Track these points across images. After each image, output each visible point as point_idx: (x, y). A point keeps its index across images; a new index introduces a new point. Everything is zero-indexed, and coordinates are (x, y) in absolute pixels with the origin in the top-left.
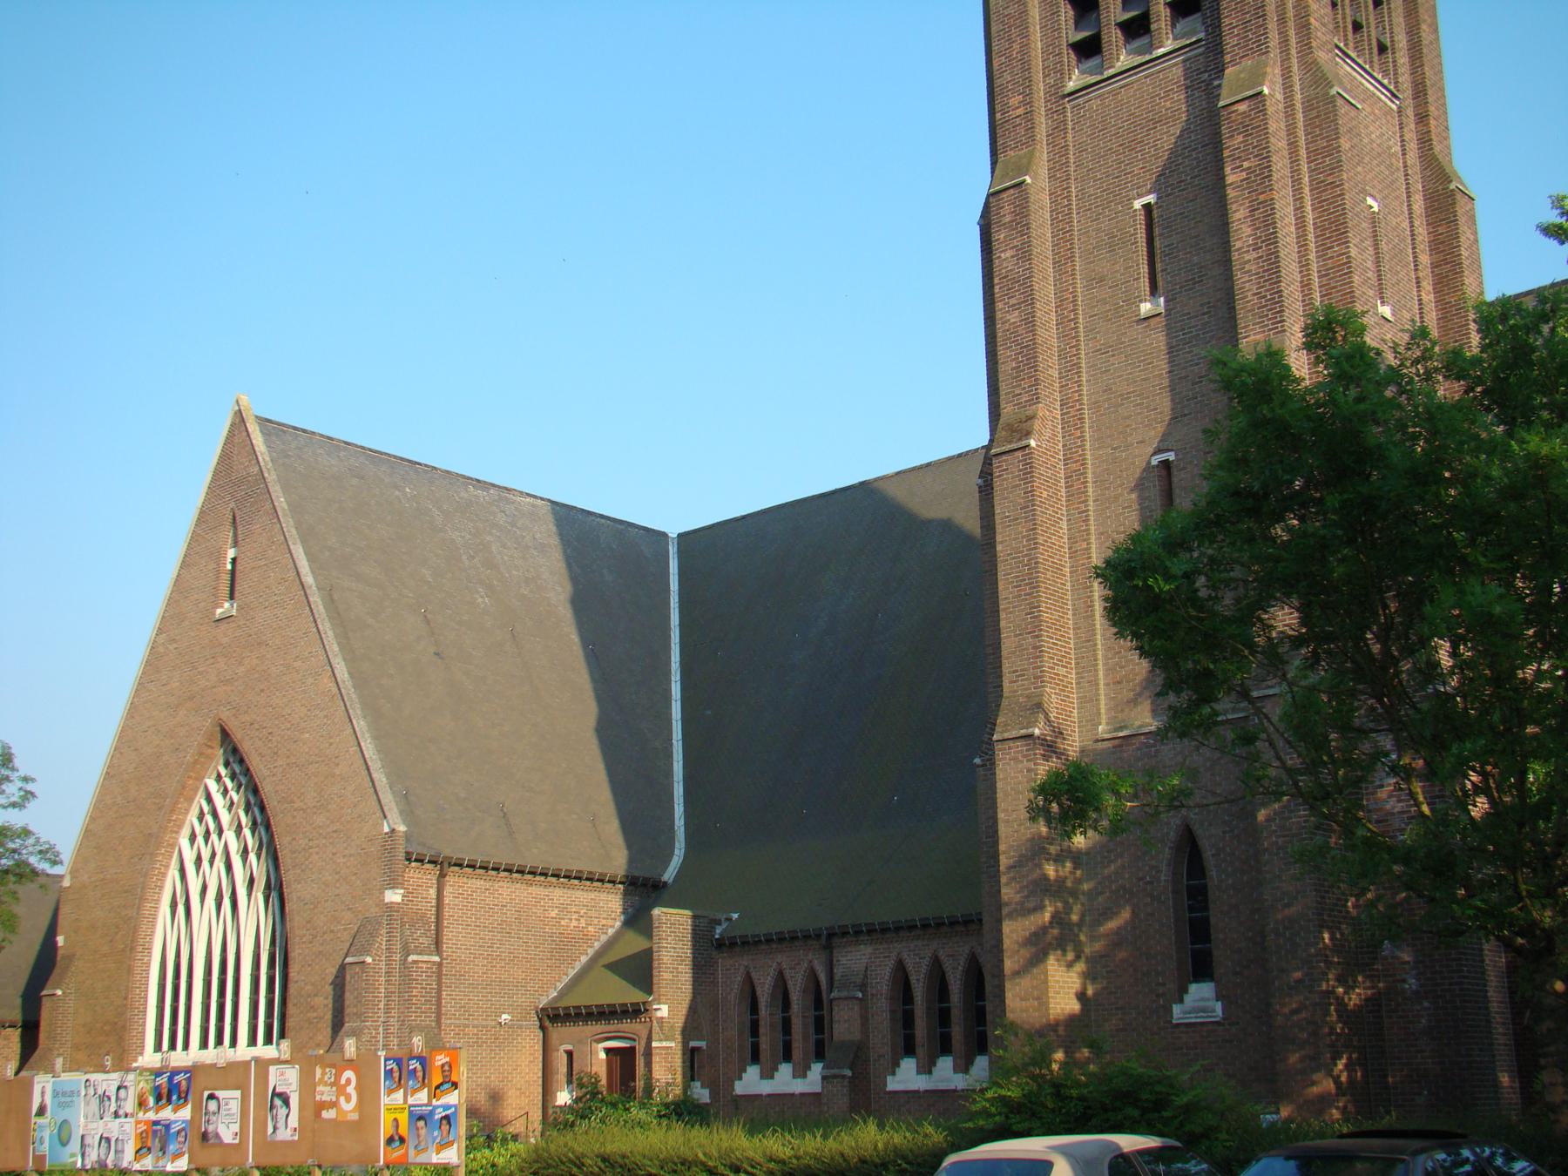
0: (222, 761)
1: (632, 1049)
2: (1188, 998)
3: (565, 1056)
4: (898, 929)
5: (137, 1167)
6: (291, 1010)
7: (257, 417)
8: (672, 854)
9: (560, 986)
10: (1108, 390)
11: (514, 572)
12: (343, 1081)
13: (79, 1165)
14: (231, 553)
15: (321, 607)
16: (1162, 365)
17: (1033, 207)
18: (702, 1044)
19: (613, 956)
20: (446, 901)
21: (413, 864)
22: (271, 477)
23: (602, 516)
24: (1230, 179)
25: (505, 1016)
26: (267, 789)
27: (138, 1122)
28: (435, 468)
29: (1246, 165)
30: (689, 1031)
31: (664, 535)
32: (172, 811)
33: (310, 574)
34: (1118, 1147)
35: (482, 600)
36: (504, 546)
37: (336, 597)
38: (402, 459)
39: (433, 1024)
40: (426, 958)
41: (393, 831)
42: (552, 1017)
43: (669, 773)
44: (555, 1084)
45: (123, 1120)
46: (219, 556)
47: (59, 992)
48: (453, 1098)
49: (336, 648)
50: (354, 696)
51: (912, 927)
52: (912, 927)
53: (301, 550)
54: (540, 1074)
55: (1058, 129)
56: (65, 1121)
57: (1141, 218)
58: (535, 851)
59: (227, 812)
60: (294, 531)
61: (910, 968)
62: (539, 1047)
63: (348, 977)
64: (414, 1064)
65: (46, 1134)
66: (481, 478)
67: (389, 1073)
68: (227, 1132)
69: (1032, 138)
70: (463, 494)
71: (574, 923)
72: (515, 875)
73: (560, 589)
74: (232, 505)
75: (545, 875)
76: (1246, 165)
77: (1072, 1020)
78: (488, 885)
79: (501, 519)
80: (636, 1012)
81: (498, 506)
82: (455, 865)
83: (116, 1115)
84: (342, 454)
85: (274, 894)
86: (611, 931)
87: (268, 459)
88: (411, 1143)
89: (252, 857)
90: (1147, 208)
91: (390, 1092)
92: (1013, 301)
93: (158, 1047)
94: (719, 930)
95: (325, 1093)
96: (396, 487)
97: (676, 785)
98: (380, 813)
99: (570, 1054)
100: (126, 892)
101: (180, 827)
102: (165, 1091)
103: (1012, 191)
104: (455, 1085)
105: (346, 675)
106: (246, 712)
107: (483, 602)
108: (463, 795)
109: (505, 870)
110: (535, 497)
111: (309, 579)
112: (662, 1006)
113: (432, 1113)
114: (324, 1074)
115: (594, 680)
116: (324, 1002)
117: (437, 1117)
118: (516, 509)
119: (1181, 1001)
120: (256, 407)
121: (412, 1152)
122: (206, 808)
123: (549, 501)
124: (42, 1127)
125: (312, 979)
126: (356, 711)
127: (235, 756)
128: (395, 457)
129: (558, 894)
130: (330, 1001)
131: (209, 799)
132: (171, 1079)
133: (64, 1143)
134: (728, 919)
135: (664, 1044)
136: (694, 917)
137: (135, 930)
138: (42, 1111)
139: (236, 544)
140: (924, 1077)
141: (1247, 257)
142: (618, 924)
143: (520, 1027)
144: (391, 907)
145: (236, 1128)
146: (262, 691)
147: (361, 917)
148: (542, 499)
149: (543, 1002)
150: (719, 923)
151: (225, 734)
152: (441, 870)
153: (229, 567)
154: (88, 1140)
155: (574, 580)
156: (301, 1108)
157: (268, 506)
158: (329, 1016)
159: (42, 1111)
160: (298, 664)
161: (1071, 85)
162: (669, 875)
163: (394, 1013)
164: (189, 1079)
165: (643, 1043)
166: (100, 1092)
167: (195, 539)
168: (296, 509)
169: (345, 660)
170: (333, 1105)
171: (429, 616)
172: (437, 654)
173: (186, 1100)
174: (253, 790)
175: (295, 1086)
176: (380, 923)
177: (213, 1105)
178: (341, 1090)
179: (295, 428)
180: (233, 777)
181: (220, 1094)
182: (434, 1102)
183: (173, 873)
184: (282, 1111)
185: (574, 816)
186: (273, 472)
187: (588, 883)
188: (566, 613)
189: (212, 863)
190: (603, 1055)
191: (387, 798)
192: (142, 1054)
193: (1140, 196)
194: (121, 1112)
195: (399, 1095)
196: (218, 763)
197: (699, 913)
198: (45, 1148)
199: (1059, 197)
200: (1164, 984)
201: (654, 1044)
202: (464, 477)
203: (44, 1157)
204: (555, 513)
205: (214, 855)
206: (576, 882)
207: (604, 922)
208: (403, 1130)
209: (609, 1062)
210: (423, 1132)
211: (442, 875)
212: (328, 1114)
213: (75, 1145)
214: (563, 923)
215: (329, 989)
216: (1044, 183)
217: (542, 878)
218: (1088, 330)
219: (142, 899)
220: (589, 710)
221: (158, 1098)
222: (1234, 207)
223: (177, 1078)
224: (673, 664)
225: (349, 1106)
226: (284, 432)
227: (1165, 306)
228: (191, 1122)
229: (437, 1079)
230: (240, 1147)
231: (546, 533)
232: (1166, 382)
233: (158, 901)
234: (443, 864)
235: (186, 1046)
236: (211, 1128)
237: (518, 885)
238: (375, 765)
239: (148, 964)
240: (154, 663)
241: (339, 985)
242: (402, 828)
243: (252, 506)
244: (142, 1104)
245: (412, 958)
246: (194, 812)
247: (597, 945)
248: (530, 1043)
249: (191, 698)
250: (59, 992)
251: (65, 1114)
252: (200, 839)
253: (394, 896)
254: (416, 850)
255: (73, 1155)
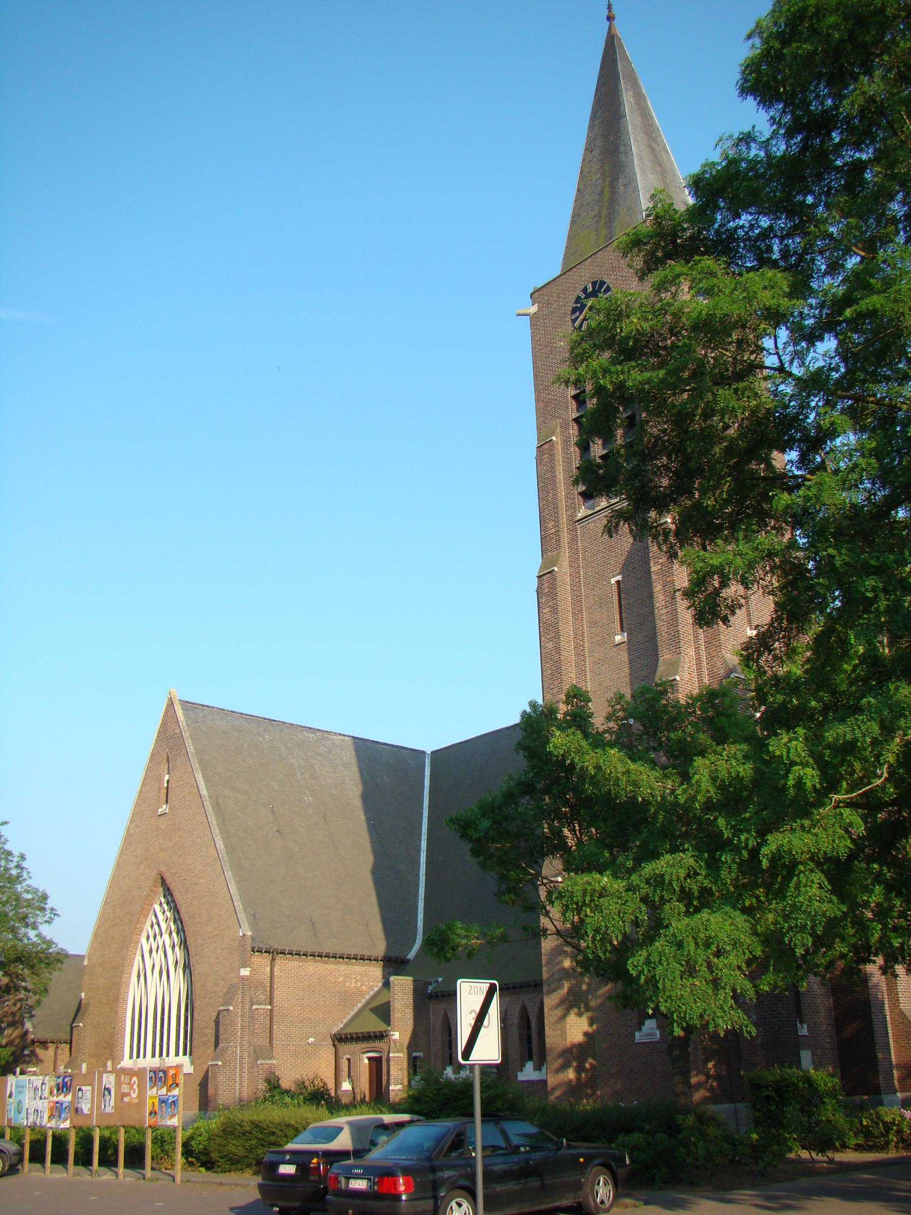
0: (162, 895)
1: (381, 1057)
2: (644, 1028)
3: (347, 1062)
4: (521, 987)
5: (49, 1125)
6: (195, 1036)
7: (180, 701)
8: (415, 942)
9: (345, 1021)
10: (600, 684)
11: (329, 781)
12: (132, 1082)
13: (25, 1124)
14: (167, 777)
15: (210, 808)
16: (627, 671)
17: (558, 584)
18: (421, 1054)
19: (375, 1004)
20: (276, 974)
21: (256, 953)
22: (186, 735)
23: (385, 744)
24: (653, 569)
25: (311, 1039)
26: (183, 910)
27: (50, 1102)
28: (284, 723)
29: (660, 561)
30: (411, 1047)
31: (424, 753)
32: (137, 923)
33: (205, 789)
34: (381, 1120)
35: (308, 798)
36: (323, 766)
37: (220, 802)
38: (265, 719)
39: (268, 1044)
40: (263, 1007)
41: (244, 935)
42: (340, 1039)
43: (416, 895)
44: (341, 1078)
45: (43, 1100)
46: (161, 779)
47: (81, 1025)
48: (176, 1092)
49: (217, 831)
50: (226, 858)
51: (529, 986)
52: (529, 986)
53: (201, 776)
54: (334, 1072)
55: (574, 540)
56: (20, 1101)
57: (615, 588)
58: (330, 944)
59: (164, 922)
60: (197, 765)
61: (529, 1009)
62: (332, 1057)
63: (221, 1018)
64: (161, 1074)
65: (12, 1107)
66: (312, 727)
67: (151, 1078)
68: (86, 1108)
69: (559, 545)
70: (301, 737)
71: (354, 985)
72: (317, 958)
73: (355, 789)
74: (167, 751)
75: (335, 957)
76: (660, 561)
77: (579, 1046)
78: (301, 964)
79: (322, 750)
80: (381, 1036)
81: (321, 743)
82: (281, 953)
83: (41, 1098)
84: (229, 718)
85: (187, 970)
86: (376, 989)
87: (185, 724)
88: (159, 1115)
89: (177, 949)
90: (618, 582)
91: (151, 1088)
92: (549, 636)
93: (131, 1057)
94: (430, 988)
95: (125, 1089)
96: (260, 735)
97: (420, 901)
98: (238, 925)
99: (349, 1060)
100: (114, 968)
101: (141, 932)
102: (61, 1086)
103: (548, 575)
104: (177, 1085)
105: (222, 846)
106: (173, 867)
107: (308, 800)
108: (288, 912)
109: (310, 955)
110: (344, 735)
111: (204, 792)
112: (395, 1033)
113: (168, 1099)
114: (125, 1078)
115: (372, 841)
116: (211, 1031)
117: (170, 1101)
118: (332, 743)
119: (640, 1030)
120: (182, 694)
121: (159, 1119)
122: (155, 921)
123: (353, 737)
124: (11, 1104)
125: (205, 1018)
126: (227, 868)
127: (168, 892)
128: (261, 718)
129: (344, 968)
130: (214, 1031)
131: (156, 916)
132: (63, 1079)
133: (20, 1112)
134: (437, 982)
135: (397, 1055)
136: (414, 981)
137: (119, 989)
138: (11, 1096)
139: (169, 773)
140: (537, 1072)
141: (662, 612)
142: (380, 984)
143: (321, 1045)
144: (244, 978)
145: (89, 1106)
146: (181, 855)
147: (229, 984)
148: (348, 736)
149: (335, 1030)
150: (430, 984)
151: (163, 881)
152: (273, 956)
153: (166, 785)
154: (29, 1111)
155: (364, 782)
156: (116, 1097)
157: (184, 751)
158: (213, 1040)
159: (11, 1096)
160: (198, 840)
161: (580, 515)
162: (411, 955)
163: (246, 1038)
164: (71, 1080)
165: (386, 1054)
166: (34, 1086)
167: (149, 770)
168: (199, 752)
169: (222, 837)
170: (128, 1094)
171: (275, 810)
172: (278, 831)
173: (69, 1090)
174: (176, 910)
175: (113, 1085)
176: (238, 987)
177: (80, 1094)
178: (132, 1087)
179: (203, 705)
180: (168, 903)
181: (84, 1088)
182: (169, 1094)
183: (138, 958)
184: (108, 1097)
185: (355, 922)
186: (187, 732)
187: (362, 961)
188: (358, 803)
189: (157, 951)
190: (366, 1061)
191: (242, 916)
192: (123, 1060)
193: (614, 576)
194: (43, 1097)
195: (155, 1090)
196: (160, 896)
197: (416, 978)
198: (12, 1115)
199: (575, 576)
200: (631, 1020)
201: (391, 1055)
202: (301, 726)
203: (11, 1119)
204: (355, 744)
205: (158, 947)
206: (354, 961)
207: (372, 983)
208: (156, 1108)
209: (370, 1065)
210: (164, 1109)
211: (273, 960)
212: (126, 1099)
213: (24, 1114)
214: (346, 984)
215: (213, 1024)
216: (567, 570)
217: (334, 959)
218: (590, 651)
219: (122, 973)
220: (368, 860)
221: (58, 1090)
222: (655, 584)
223: (66, 1079)
224: (423, 830)
225: (134, 1095)
226: (196, 708)
227: (628, 637)
228: (70, 1102)
229: (170, 1082)
230: (90, 1116)
231: (349, 756)
232: (628, 680)
233: (131, 973)
234: (273, 953)
235: (145, 1057)
236: (79, 1106)
237: (319, 964)
238: (236, 898)
239: (126, 1009)
240: (128, 839)
241: (217, 1022)
242: (249, 933)
243: (177, 750)
244: (51, 1092)
245: (254, 1007)
246: (149, 923)
247: (367, 997)
248: (328, 1053)
249: (146, 859)
250: (81, 1025)
251: (20, 1097)
252: (152, 938)
253: (245, 972)
254: (257, 945)
255: (23, 1119)
